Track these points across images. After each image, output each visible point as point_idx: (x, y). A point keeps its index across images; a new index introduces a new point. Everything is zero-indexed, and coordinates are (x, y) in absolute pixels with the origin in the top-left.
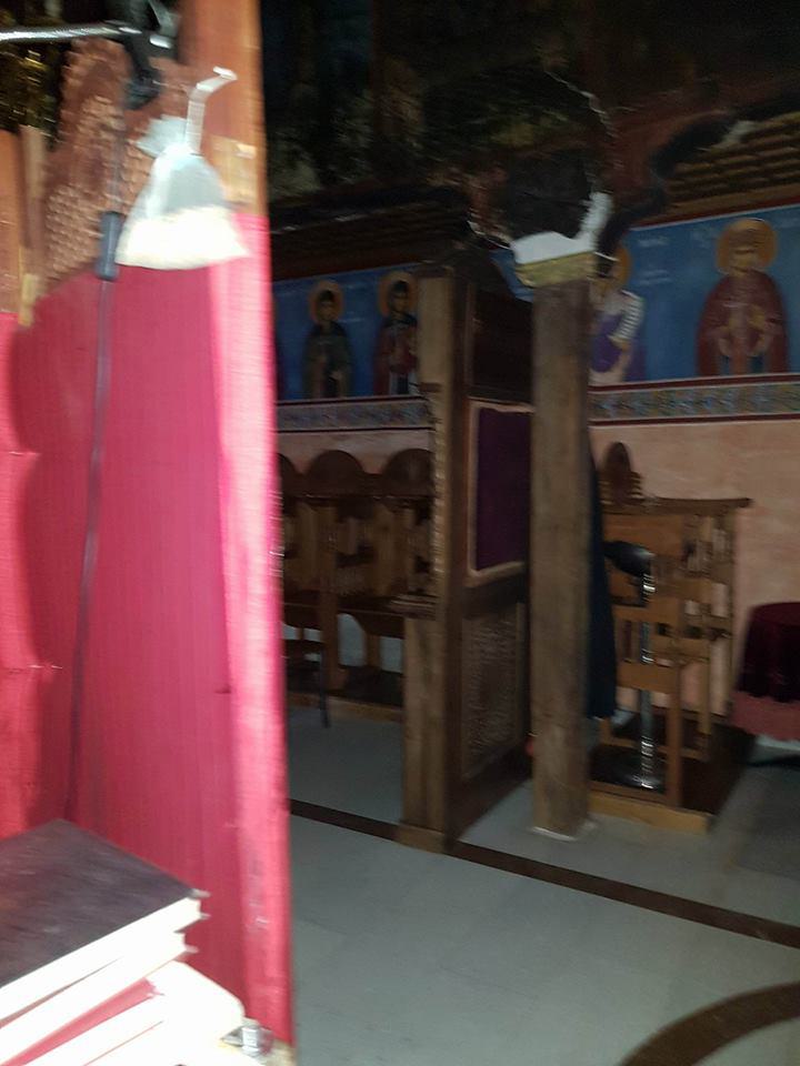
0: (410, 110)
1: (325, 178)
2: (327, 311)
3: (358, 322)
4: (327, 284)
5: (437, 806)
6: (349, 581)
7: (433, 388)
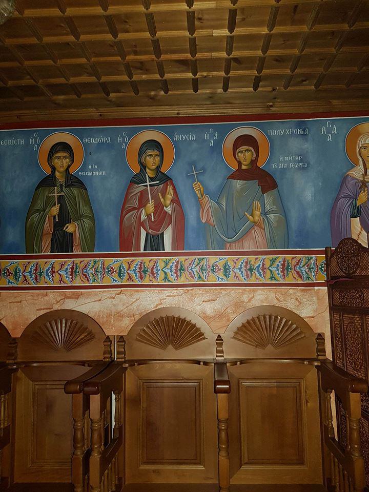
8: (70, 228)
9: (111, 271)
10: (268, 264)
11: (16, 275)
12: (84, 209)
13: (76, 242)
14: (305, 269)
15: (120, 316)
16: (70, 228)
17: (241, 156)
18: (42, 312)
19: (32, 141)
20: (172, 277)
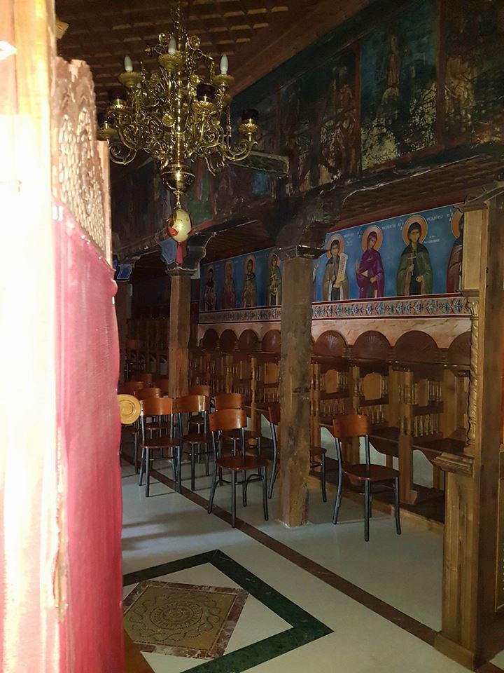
0: (464, 91)
1: (403, 148)
2: (414, 237)
3: (435, 242)
4: (415, 218)
5: (468, 632)
6: (426, 424)
7: (474, 293)
8: (419, 279)
9: (442, 306)
10: (412, 304)
11: (447, 308)
12: (427, 266)
13: (423, 287)
14: (430, 307)
15: (446, 336)
16: (419, 279)
17: (412, 237)
18: (405, 332)
19: (399, 224)
20: (456, 311)
